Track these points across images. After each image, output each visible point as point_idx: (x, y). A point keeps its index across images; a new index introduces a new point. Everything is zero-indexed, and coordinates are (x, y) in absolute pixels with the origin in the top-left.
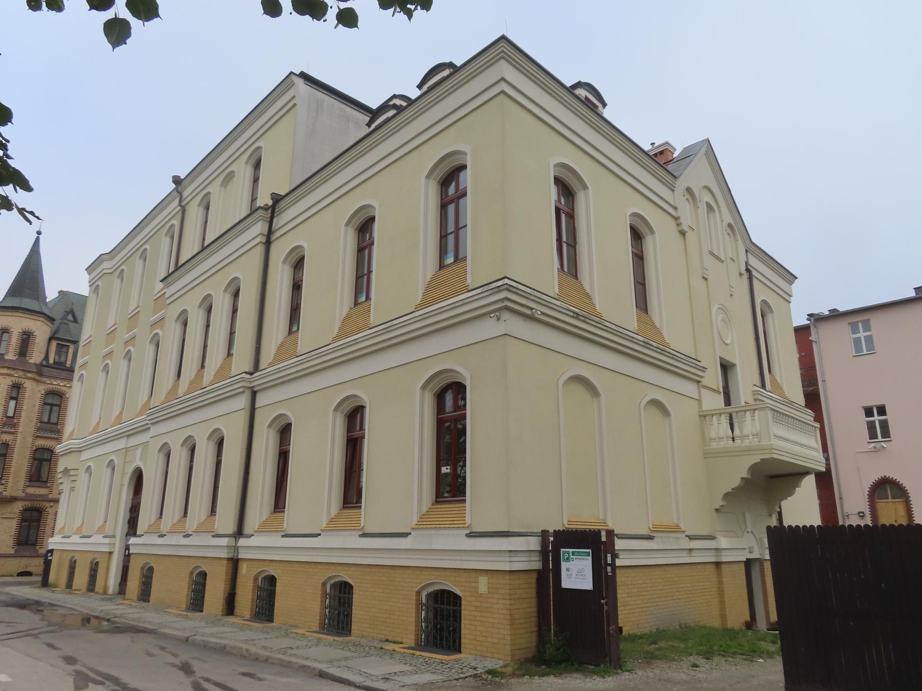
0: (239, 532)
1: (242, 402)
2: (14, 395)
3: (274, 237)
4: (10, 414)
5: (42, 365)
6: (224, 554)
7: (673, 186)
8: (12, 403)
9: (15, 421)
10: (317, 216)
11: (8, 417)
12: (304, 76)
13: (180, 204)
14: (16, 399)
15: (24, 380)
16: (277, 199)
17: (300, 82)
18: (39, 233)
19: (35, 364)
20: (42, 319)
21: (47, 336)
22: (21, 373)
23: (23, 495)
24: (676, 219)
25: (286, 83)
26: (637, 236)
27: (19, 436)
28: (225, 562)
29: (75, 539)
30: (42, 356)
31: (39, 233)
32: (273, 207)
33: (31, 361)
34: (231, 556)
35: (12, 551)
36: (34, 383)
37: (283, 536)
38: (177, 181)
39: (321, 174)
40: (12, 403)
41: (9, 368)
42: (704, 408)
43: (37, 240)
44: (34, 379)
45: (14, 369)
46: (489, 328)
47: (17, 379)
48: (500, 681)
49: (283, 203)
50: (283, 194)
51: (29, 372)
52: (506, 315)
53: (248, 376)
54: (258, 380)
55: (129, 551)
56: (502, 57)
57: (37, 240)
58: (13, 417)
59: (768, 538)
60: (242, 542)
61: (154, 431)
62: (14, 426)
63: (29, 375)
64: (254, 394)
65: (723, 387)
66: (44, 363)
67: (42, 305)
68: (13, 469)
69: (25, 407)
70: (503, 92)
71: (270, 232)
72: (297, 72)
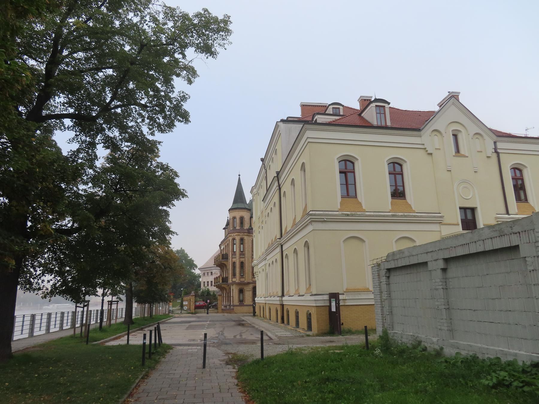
0: (283, 295)
1: (278, 249)
2: (242, 243)
3: (281, 186)
4: (242, 250)
5: (249, 229)
6: (278, 303)
7: (97, 313)
8: (242, 246)
9: (244, 253)
10: (333, 145)
11: (241, 251)
12: (282, 121)
13: (265, 170)
14: (242, 244)
15: (244, 236)
16: (278, 173)
17: (281, 124)
18: (239, 175)
19: (247, 229)
20: (246, 211)
21: (249, 217)
22: (242, 234)
23: (252, 281)
24: (425, 149)
25: (277, 126)
26: (455, 136)
27: (246, 258)
28: (280, 305)
29: (296, 298)
30: (249, 225)
31: (239, 175)
32: (277, 176)
33: (245, 228)
34: (281, 303)
35: (238, 304)
36: (248, 237)
37: (298, 296)
38: (262, 160)
39: (286, 162)
40: (242, 246)
41: (238, 232)
42: (443, 234)
43: (239, 178)
44: (247, 235)
45: (240, 232)
46: (310, 228)
47: (241, 236)
48: (452, 364)
49: (280, 174)
50: (279, 171)
51: (245, 233)
52: (313, 223)
53: (279, 240)
54: (282, 241)
55: (88, 309)
56: (307, 130)
57: (239, 178)
58: (243, 251)
59: (126, 308)
60: (284, 298)
61: (268, 258)
62: (244, 255)
63: (245, 234)
64: (282, 246)
65: (462, 220)
66: (250, 228)
67: (245, 205)
68: (246, 272)
69: (246, 247)
70: (308, 142)
71: (279, 185)
72: (279, 120)
